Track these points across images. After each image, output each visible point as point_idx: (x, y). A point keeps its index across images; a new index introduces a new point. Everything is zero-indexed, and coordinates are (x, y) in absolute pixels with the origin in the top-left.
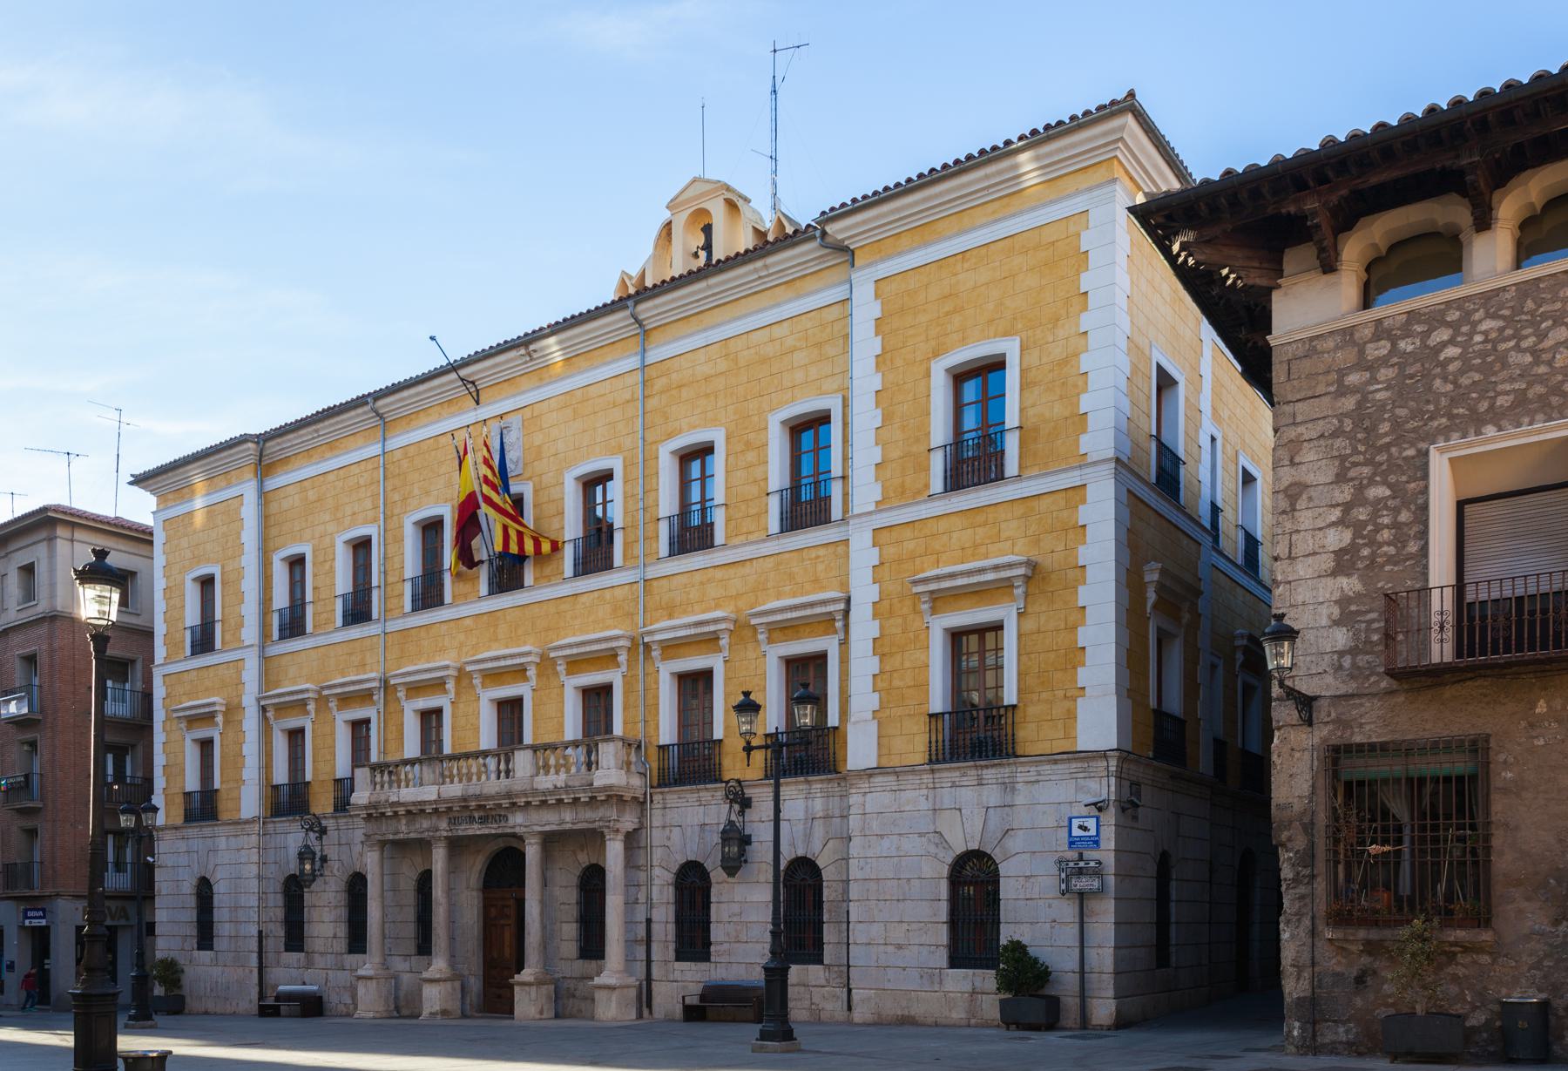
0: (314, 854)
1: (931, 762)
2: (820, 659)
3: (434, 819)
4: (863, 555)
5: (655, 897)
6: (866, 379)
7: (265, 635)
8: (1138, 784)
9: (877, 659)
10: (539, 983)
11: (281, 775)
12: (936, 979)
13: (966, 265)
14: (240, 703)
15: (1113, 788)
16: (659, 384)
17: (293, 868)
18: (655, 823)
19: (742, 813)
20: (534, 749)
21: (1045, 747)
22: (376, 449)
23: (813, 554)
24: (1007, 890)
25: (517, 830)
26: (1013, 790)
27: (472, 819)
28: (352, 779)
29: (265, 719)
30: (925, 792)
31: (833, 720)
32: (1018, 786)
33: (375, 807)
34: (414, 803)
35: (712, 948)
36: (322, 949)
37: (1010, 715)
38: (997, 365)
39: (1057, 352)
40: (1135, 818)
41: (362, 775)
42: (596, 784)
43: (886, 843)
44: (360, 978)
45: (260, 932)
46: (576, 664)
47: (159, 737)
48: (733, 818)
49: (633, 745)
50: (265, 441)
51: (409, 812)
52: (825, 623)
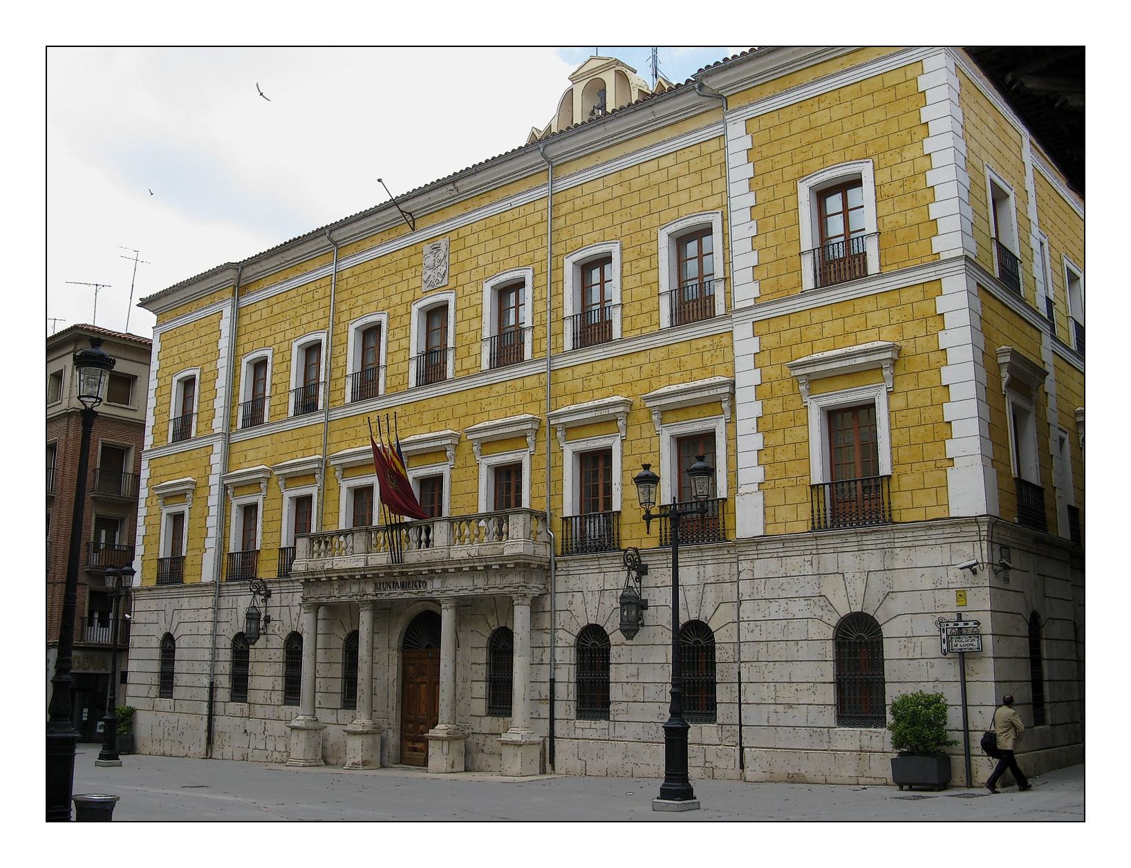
0: (260, 614)
1: (813, 528)
2: (708, 438)
4: (745, 343)
5: (558, 658)
6: (742, 199)
8: (1007, 548)
9: (760, 436)
10: (450, 739)
11: (234, 545)
12: (825, 738)
13: (822, 106)
15: (985, 552)
19: (639, 579)
20: (451, 521)
21: (918, 515)
22: (330, 270)
23: (700, 344)
24: (890, 649)
25: (435, 595)
27: (395, 584)
28: (294, 548)
31: (722, 492)
33: (312, 573)
35: (612, 707)
36: (261, 701)
37: (885, 485)
39: (906, 170)
40: (1006, 580)
41: (302, 544)
44: (293, 728)
45: (212, 683)
46: (488, 445)
47: (142, 512)
48: (631, 583)
49: (541, 517)
51: (341, 578)
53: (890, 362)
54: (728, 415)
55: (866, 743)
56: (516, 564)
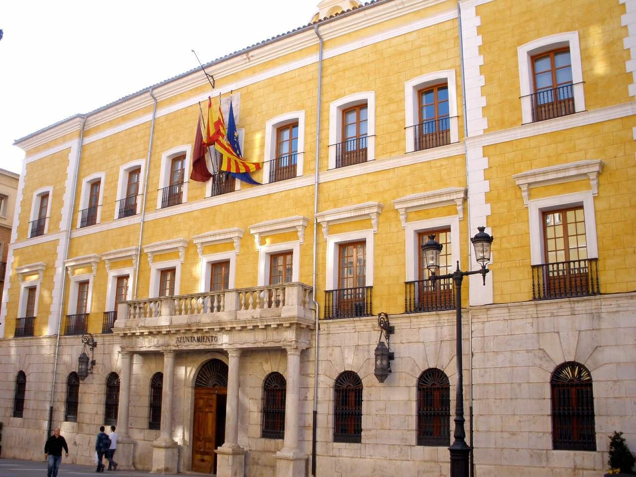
0: (88, 359)
1: (534, 299)
3: (167, 337)
6: (473, 60)
7: (73, 226)
14: (54, 265)
16: (330, 70)
17: (75, 368)
18: (321, 345)
19: (388, 337)
20: (238, 292)
25: (224, 347)
26: (599, 318)
28: (115, 313)
29: (67, 275)
30: (530, 320)
32: (603, 315)
34: (155, 327)
35: (363, 433)
38: (564, 49)
42: (283, 316)
43: (501, 357)
45: (52, 408)
49: (307, 290)
50: (88, 117)
52: (449, 207)
53: (595, 174)
54: (461, 215)
55: (579, 462)
56: (291, 324)
